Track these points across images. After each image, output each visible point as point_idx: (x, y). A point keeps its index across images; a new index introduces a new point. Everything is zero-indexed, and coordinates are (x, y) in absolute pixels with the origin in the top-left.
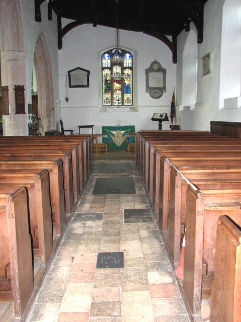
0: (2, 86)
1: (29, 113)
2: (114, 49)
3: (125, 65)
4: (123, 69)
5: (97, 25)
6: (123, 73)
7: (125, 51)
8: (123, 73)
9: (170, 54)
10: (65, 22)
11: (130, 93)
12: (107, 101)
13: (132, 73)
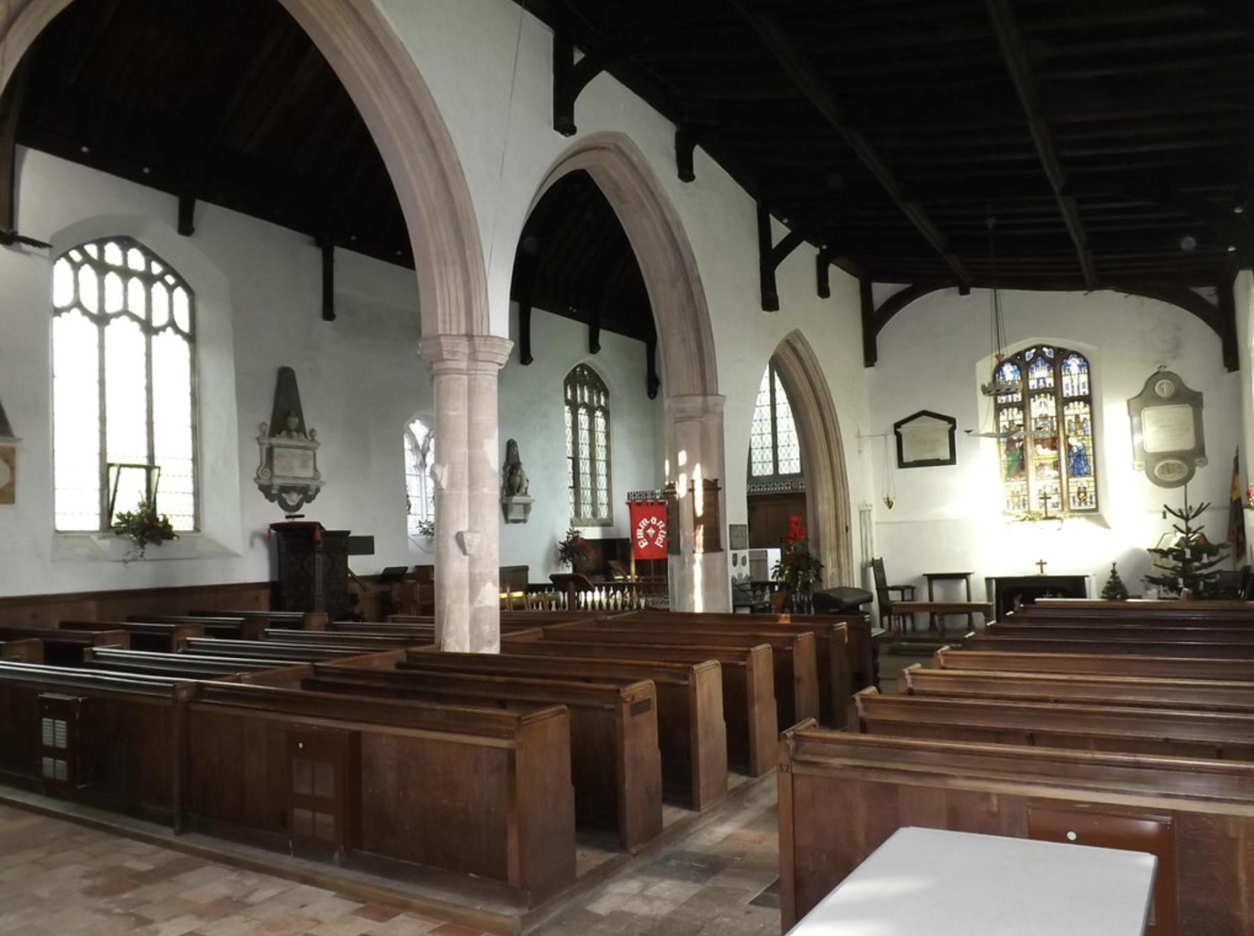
0: (62, 524)
1: (732, 548)
2: (1029, 349)
3: (1067, 392)
4: (1063, 402)
5: (973, 290)
6: (1060, 416)
7: (1063, 350)
8: (1060, 416)
9: (1212, 342)
10: (882, 291)
11: (1087, 474)
12: (1016, 500)
13: (1091, 413)
